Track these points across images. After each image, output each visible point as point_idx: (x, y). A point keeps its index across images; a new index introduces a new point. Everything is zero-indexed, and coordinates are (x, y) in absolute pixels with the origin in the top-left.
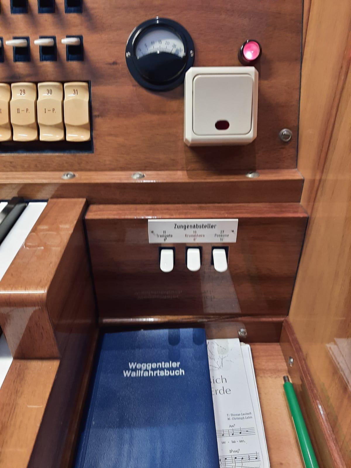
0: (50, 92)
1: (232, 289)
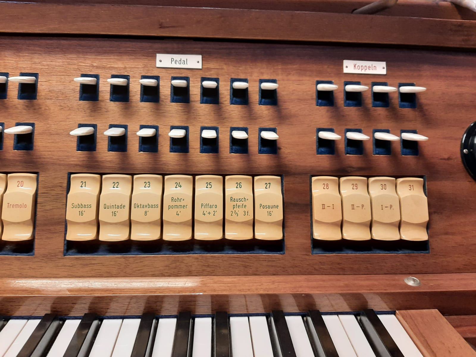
0: (239, 185)
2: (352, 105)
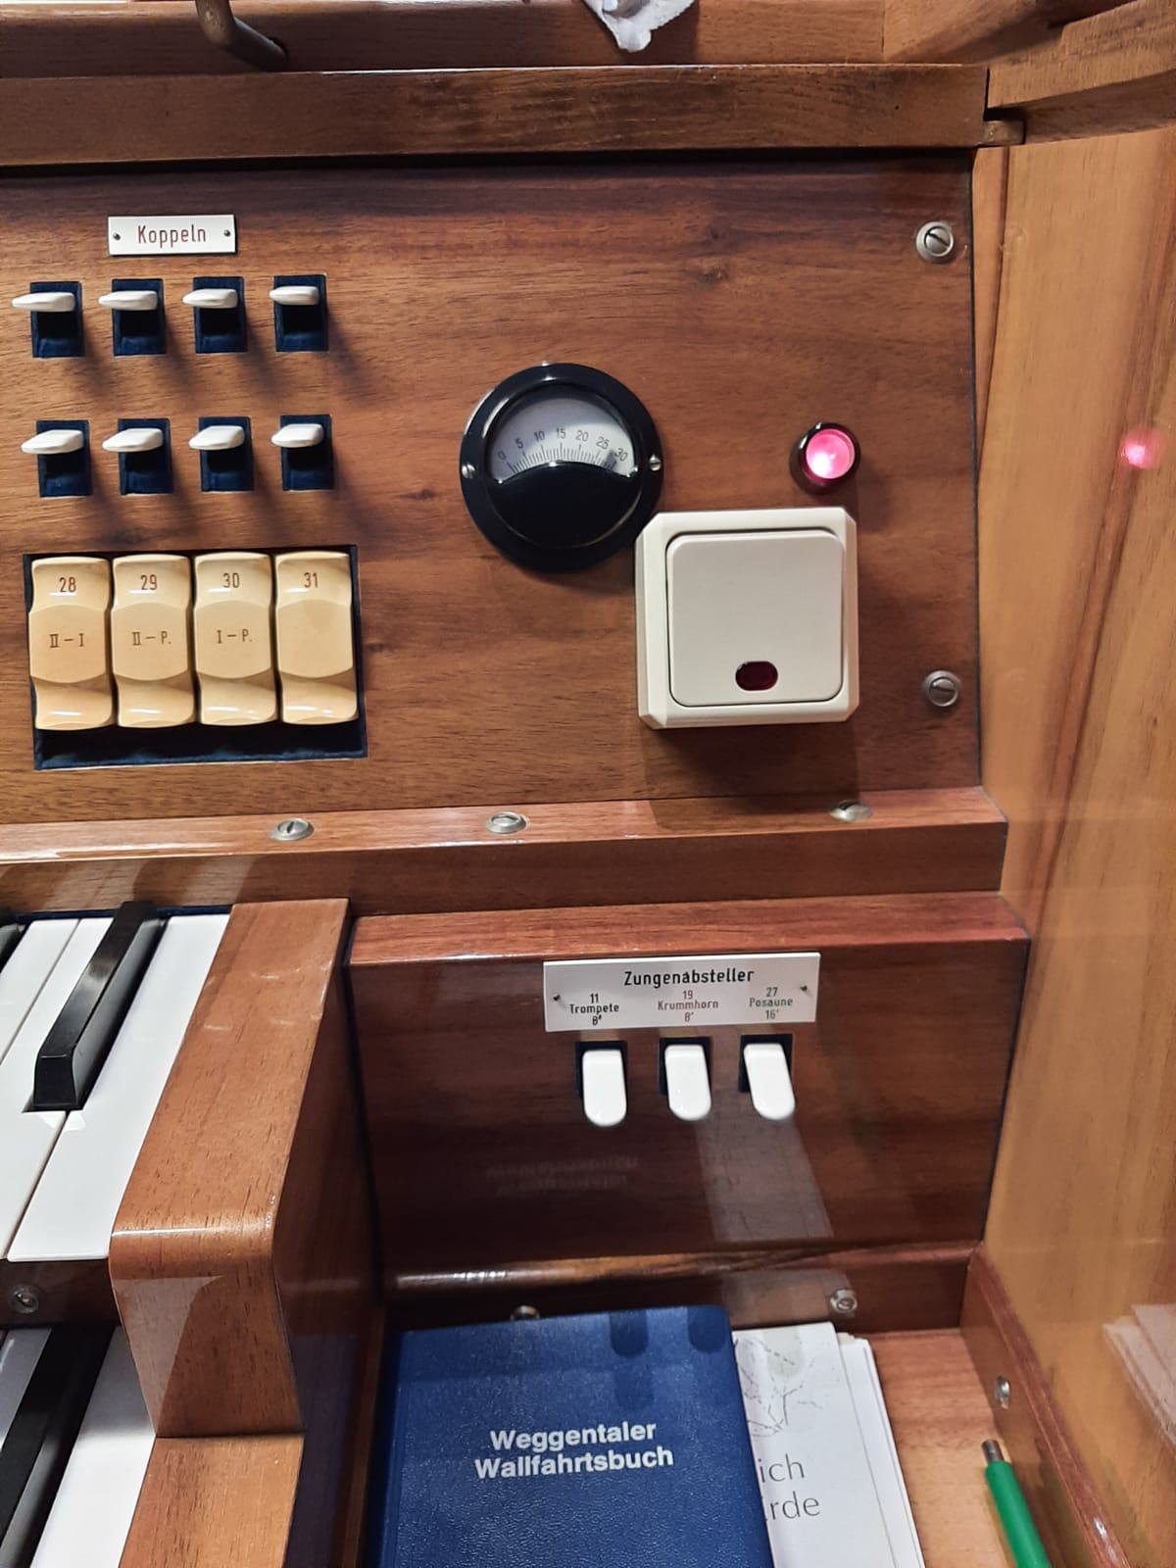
0: (232, 580)
1: (802, 1167)
2: (137, 349)
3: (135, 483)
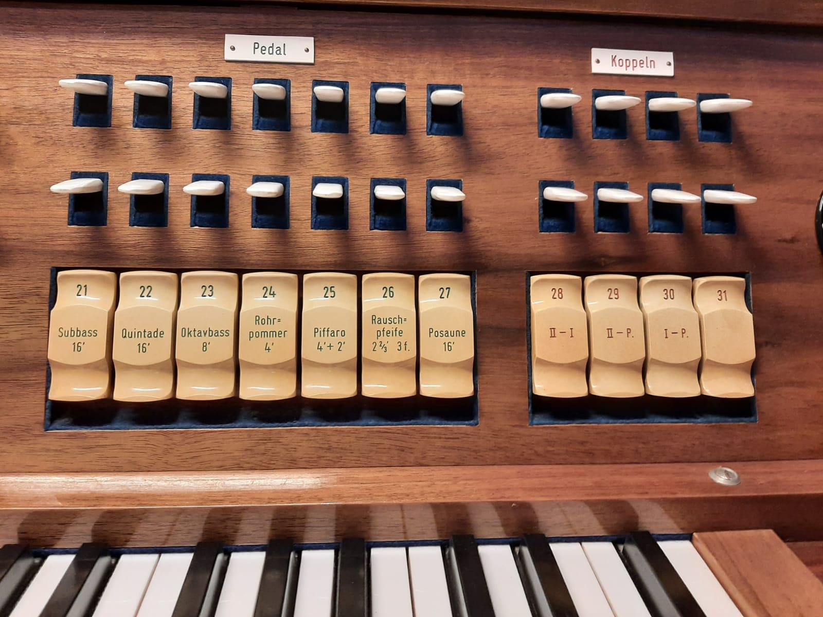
3: (605, 226)
